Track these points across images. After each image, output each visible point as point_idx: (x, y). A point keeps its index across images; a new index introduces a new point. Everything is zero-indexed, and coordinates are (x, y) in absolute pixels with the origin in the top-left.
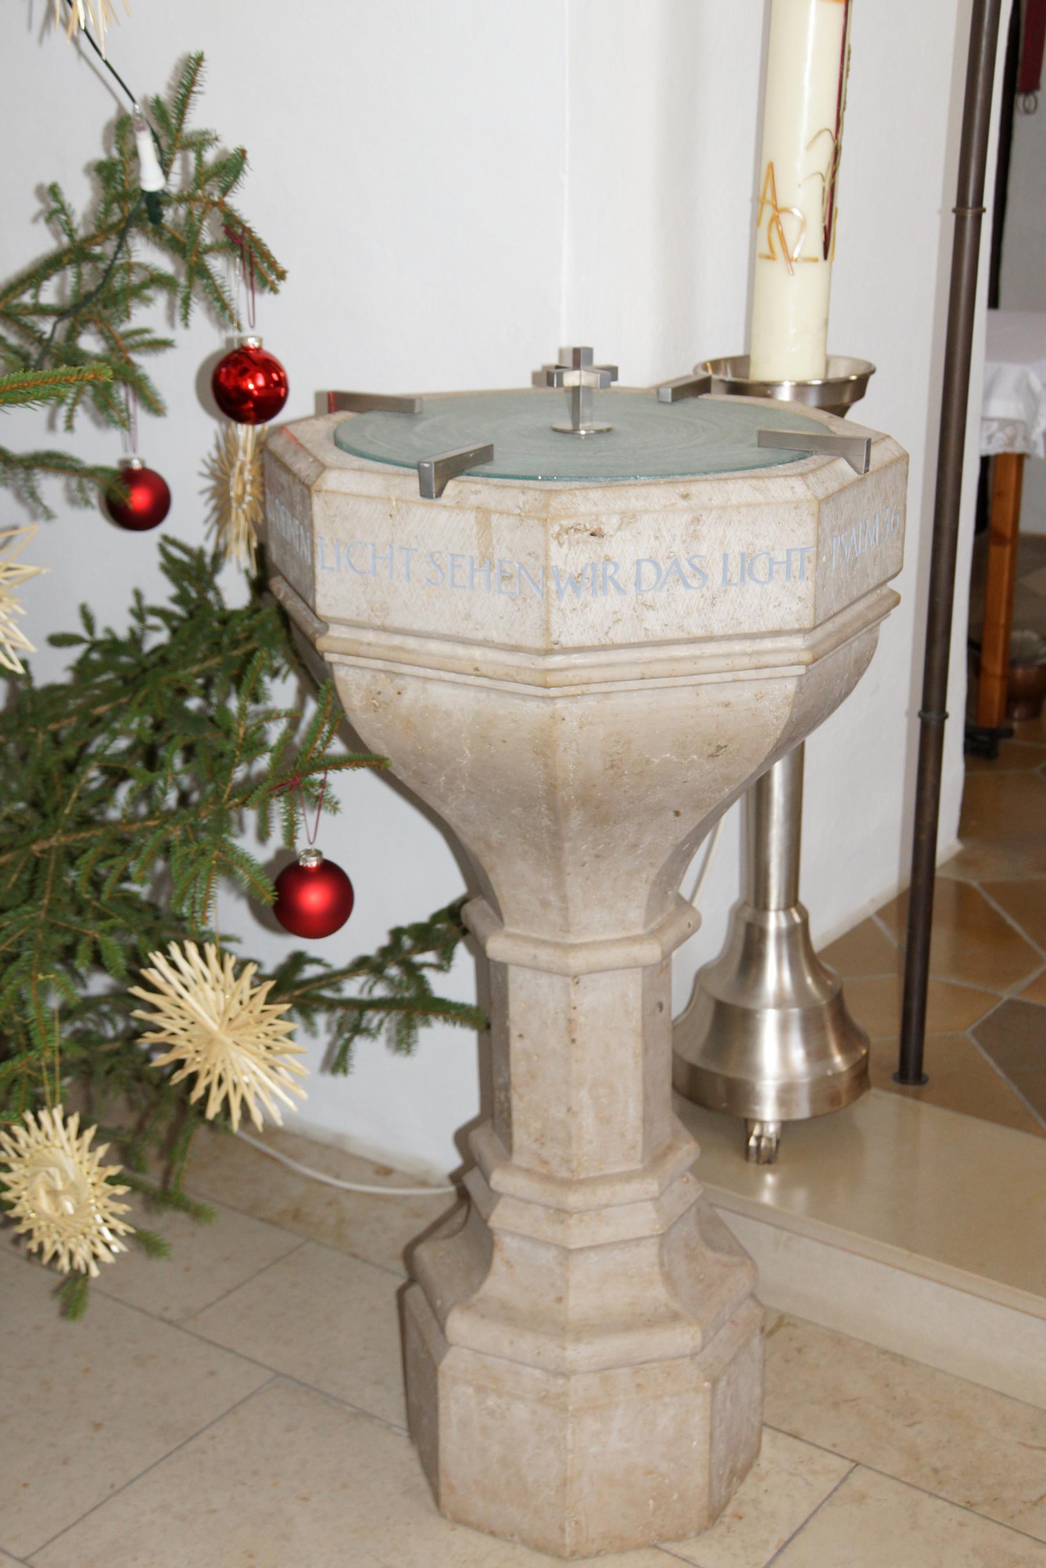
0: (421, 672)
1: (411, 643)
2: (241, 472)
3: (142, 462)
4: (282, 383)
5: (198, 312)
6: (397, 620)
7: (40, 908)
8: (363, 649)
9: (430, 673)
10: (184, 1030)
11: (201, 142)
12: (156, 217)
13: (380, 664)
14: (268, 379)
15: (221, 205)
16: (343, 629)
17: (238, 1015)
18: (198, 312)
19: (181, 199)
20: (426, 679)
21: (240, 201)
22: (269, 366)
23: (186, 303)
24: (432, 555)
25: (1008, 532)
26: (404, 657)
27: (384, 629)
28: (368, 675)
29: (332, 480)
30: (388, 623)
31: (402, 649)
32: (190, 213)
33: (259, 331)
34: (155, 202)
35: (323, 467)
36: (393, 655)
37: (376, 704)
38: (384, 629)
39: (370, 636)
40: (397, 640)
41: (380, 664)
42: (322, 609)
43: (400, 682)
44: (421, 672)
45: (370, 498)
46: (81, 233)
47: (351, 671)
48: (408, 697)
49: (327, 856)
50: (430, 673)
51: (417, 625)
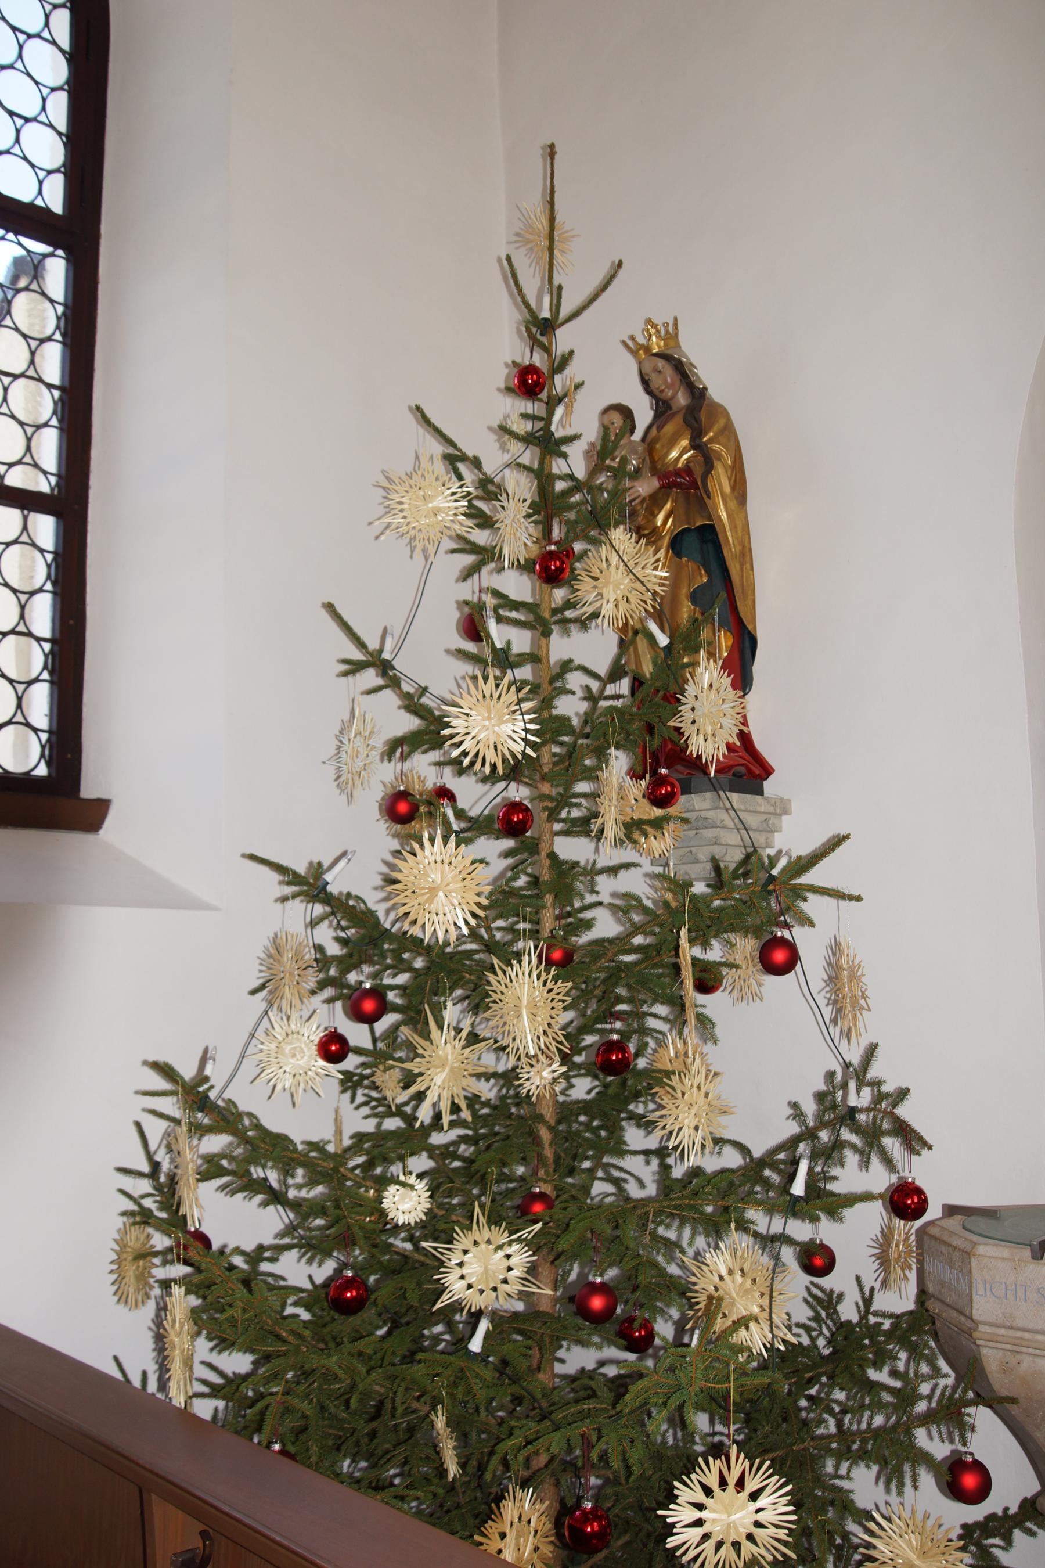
0: (1033, 1351)
1: (1027, 1335)
2: (897, 1246)
3: (821, 1240)
4: (926, 1201)
5: (875, 1161)
6: (1020, 1323)
7: (808, 1480)
8: (1000, 1339)
9: (1038, 1352)
10: (892, 1560)
11: (877, 1083)
12: (853, 1118)
13: (1008, 1347)
14: (919, 1198)
15: (892, 1113)
16: (987, 1327)
17: (930, 1549)
18: (875, 1161)
19: (868, 1110)
20: (1035, 1355)
21: (903, 1111)
22: (919, 1192)
23: (869, 1158)
24: (1039, 1289)
25: (563, 525)
26: (1024, 1343)
27: (1012, 1328)
28: (1001, 1353)
29: (981, 1250)
30: (1014, 1324)
31: (1022, 1339)
32: (875, 1118)
33: (913, 1174)
34: (853, 1111)
35: (975, 1244)
36: (1018, 1342)
37: (1006, 1369)
38: (1012, 1328)
39: (1002, 1331)
40: (1019, 1334)
41: (1008, 1347)
42: (977, 1315)
43: (1019, 1357)
44: (1033, 1351)
45: (1003, 1259)
46: (811, 1124)
47: (991, 1350)
48: (1025, 1365)
49: (976, 1457)
50: (1038, 1352)
51: (1031, 1326)
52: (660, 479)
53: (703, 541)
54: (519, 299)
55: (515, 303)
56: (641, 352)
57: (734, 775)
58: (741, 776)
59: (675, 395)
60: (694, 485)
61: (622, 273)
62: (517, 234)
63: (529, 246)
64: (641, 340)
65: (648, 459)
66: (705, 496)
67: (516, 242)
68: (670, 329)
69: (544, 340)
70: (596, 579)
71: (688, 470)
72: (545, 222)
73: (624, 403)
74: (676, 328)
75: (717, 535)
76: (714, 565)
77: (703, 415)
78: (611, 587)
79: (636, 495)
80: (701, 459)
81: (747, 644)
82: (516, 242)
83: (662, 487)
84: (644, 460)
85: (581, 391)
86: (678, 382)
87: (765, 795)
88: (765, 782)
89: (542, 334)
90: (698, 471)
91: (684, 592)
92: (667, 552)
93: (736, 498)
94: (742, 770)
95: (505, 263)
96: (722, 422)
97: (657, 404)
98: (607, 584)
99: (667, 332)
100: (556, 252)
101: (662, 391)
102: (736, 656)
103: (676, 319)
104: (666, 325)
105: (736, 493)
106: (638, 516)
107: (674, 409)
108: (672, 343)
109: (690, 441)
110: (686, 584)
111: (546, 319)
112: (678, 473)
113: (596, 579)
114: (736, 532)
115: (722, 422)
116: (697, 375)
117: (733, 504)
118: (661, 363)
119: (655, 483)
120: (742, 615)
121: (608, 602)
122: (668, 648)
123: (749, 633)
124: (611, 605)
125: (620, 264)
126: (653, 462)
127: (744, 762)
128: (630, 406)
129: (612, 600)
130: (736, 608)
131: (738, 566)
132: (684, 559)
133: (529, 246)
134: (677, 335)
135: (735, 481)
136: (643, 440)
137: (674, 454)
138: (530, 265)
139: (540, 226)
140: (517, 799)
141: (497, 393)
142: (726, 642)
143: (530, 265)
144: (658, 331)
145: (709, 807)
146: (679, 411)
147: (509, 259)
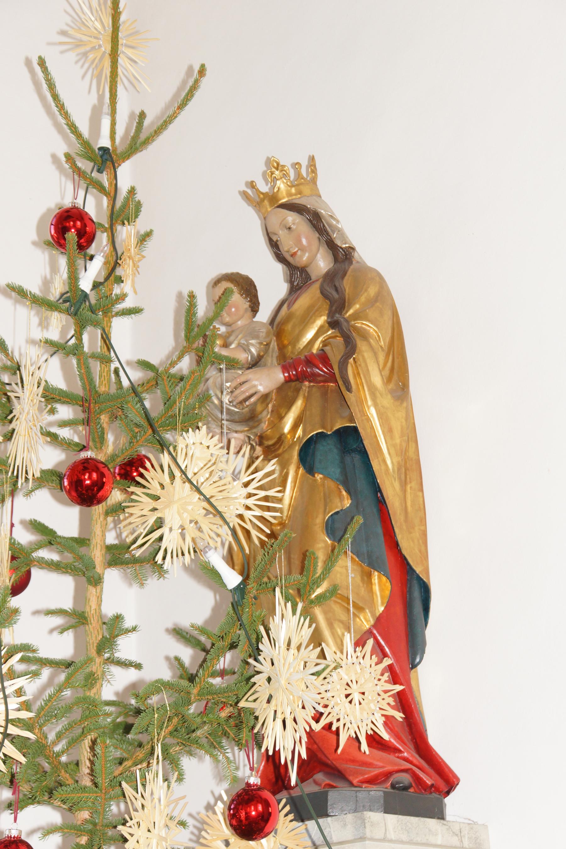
52: (285, 369)
53: (345, 450)
54: (63, 121)
55: (57, 125)
56: (266, 202)
57: (393, 786)
58: (405, 788)
59: (313, 258)
60: (332, 377)
61: (204, 82)
62: (63, 33)
63: (82, 50)
64: (264, 188)
65: (274, 344)
66: (343, 389)
67: (61, 43)
68: (304, 172)
69: (104, 178)
70: (156, 498)
71: (324, 358)
72: (108, 21)
73: (243, 272)
74: (314, 171)
75: (362, 440)
76: (362, 484)
77: (347, 284)
78: (175, 507)
79: (252, 391)
80: (340, 340)
81: (417, 594)
82: (61, 43)
83: (288, 380)
84: (268, 345)
85: (150, 244)
86: (315, 243)
87: (448, 818)
88: (448, 800)
89: (100, 171)
90: (335, 357)
91: (320, 520)
92: (298, 468)
93: (391, 392)
94: (406, 778)
95: (38, 69)
96: (372, 291)
97: (291, 276)
98: (169, 505)
99: (298, 175)
100: (122, 61)
101: (293, 255)
102: (399, 610)
103: (312, 159)
104: (296, 165)
105: (391, 386)
106: (260, 422)
107: (313, 278)
108: (306, 190)
109: (328, 317)
110: (321, 510)
111: (104, 150)
112: (309, 361)
113: (156, 498)
114: (392, 438)
115: (372, 291)
116: (339, 230)
117: (387, 401)
118: (291, 218)
119: (280, 376)
120: (405, 552)
121: (171, 529)
122: (241, 589)
123: (420, 579)
124: (177, 532)
125: (202, 71)
126: (282, 348)
127: (409, 766)
128: (251, 276)
129: (176, 527)
130: (397, 544)
131: (397, 485)
132: (319, 477)
133: (82, 50)
134: (314, 181)
135: (392, 370)
136: (272, 322)
137: (310, 335)
138: (83, 77)
139: (98, 25)
140: (14, 833)
141: (33, 247)
142: (382, 590)
143: (83, 77)
144: (285, 175)
145: (350, 837)
146: (317, 280)
147: (42, 62)
